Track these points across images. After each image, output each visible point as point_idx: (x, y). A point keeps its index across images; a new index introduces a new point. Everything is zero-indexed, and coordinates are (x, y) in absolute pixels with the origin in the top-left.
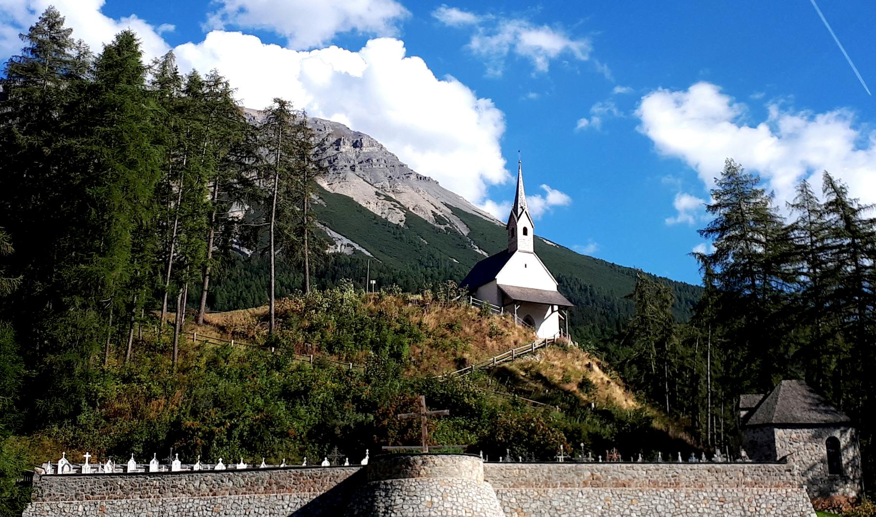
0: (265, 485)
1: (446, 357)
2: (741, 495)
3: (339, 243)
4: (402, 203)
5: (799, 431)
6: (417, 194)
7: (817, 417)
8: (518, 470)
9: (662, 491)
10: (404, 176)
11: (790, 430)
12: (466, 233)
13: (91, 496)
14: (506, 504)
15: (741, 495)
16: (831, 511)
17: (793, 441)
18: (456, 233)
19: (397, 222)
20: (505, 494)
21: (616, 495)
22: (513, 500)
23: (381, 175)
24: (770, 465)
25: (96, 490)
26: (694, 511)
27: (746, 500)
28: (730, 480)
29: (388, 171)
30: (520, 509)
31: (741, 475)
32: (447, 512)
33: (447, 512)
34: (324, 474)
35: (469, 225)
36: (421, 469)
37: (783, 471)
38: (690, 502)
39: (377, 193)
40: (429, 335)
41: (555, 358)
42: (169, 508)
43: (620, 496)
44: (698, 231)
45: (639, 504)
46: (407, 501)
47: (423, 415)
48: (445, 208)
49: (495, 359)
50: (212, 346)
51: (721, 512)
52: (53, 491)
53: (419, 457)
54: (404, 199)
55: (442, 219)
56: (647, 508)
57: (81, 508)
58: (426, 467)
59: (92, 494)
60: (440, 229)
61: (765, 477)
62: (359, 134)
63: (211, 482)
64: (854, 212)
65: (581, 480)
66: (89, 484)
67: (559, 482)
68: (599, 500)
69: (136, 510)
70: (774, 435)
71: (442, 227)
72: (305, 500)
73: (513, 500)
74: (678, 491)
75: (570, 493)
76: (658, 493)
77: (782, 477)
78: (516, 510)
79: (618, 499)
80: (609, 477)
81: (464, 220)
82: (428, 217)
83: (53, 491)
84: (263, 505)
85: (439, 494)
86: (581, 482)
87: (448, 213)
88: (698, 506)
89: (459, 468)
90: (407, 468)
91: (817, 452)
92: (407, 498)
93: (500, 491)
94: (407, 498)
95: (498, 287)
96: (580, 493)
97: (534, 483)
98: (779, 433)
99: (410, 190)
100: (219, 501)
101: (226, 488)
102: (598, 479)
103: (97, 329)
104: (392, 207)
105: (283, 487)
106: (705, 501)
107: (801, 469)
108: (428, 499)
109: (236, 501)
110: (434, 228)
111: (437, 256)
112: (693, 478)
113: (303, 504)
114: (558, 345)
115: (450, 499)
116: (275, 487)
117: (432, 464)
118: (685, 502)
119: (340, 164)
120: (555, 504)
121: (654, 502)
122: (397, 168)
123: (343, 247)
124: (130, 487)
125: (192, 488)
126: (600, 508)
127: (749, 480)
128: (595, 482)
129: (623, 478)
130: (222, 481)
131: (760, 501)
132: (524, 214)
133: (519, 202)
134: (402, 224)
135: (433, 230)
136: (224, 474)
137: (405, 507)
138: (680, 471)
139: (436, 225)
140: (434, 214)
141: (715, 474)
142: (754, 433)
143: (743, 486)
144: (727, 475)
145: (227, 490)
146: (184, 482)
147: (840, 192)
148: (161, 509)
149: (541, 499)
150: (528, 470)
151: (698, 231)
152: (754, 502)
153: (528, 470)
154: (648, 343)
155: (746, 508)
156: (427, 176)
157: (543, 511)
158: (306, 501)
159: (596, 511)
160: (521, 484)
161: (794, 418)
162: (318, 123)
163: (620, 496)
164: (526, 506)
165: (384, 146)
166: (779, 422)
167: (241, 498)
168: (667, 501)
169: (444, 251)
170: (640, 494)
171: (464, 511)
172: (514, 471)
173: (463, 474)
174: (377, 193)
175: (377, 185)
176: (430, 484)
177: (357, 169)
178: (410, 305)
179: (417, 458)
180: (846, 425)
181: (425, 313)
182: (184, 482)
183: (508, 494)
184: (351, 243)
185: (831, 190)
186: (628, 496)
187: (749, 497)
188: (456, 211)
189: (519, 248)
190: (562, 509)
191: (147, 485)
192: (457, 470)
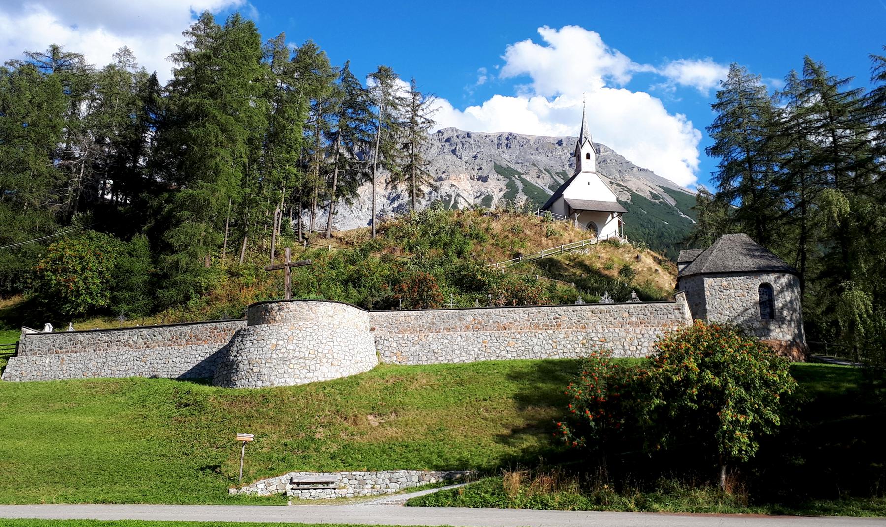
0: (186, 338)
1: (503, 253)
5: (729, 279)
7: (750, 263)
8: (403, 318)
9: (540, 332)
11: (721, 279)
12: (674, 204)
13: (59, 350)
14: (387, 349)
15: (623, 334)
17: (723, 289)
18: (666, 205)
19: (626, 200)
20: (387, 340)
21: (494, 338)
22: (394, 345)
23: (614, 170)
24: (657, 304)
25: (63, 346)
26: (571, 351)
28: (613, 321)
29: (618, 167)
30: (400, 353)
31: (626, 315)
34: (234, 327)
35: (677, 199)
36: (277, 315)
37: (672, 310)
38: (568, 342)
39: (611, 182)
40: (494, 236)
42: (109, 359)
43: (497, 338)
44: (706, 128)
45: (516, 346)
46: (255, 344)
47: (286, 265)
48: (659, 189)
49: (543, 254)
52: (33, 347)
53: (276, 304)
54: (630, 185)
56: (523, 349)
57: (48, 360)
58: (281, 313)
59: (61, 348)
61: (652, 316)
62: (597, 145)
63: (146, 336)
65: (463, 324)
66: (58, 340)
67: (442, 327)
68: (476, 342)
70: (703, 284)
71: (657, 201)
72: (214, 350)
73: (394, 345)
74: (557, 332)
75: (449, 337)
76: (537, 334)
77: (670, 316)
78: (396, 354)
79: (495, 341)
80: (491, 321)
81: (673, 195)
82: (648, 196)
83: (33, 347)
84: (180, 355)
85: (286, 337)
86: (463, 327)
87: (660, 191)
88: (576, 346)
89: (315, 314)
90: (265, 314)
91: (748, 298)
92: (256, 342)
93: (383, 337)
94: (256, 342)
95: (565, 202)
96: (459, 337)
97: (418, 329)
98: (708, 281)
99: (634, 178)
101: (157, 341)
102: (480, 323)
104: (621, 190)
105: (200, 339)
107: (731, 315)
108: (274, 342)
109: (160, 352)
110: (651, 202)
111: (653, 220)
112: (575, 319)
113: (211, 354)
114: (610, 242)
116: (194, 339)
117: (287, 310)
118: (563, 343)
121: (531, 343)
122: (624, 165)
124: (87, 342)
125: (132, 342)
126: (476, 350)
127: (634, 319)
128: (477, 326)
130: (154, 336)
131: (643, 340)
132: (587, 143)
133: (583, 133)
134: (629, 201)
136: (155, 329)
138: (563, 313)
139: (652, 200)
140: (651, 193)
141: (599, 315)
142: (686, 283)
143: (628, 326)
144: (611, 316)
145: (157, 343)
146: (126, 337)
148: (104, 360)
149: (421, 343)
150: (413, 317)
151: (706, 128)
152: (636, 341)
153: (413, 317)
154: (706, 242)
155: (627, 348)
157: (421, 355)
158: (215, 350)
159: (472, 353)
160: (406, 330)
161: (725, 267)
163: (497, 338)
164: (406, 349)
165: (615, 151)
166: (709, 271)
168: (545, 342)
169: (659, 217)
170: (518, 336)
171: (307, 353)
172: (400, 319)
173: (320, 319)
174: (611, 182)
175: (611, 177)
176: (280, 328)
179: (274, 305)
180: (782, 271)
182: (126, 337)
183: (390, 339)
186: (506, 338)
187: (630, 336)
188: (667, 190)
189: (583, 169)
190: (439, 352)
191: (99, 340)
192: (313, 315)
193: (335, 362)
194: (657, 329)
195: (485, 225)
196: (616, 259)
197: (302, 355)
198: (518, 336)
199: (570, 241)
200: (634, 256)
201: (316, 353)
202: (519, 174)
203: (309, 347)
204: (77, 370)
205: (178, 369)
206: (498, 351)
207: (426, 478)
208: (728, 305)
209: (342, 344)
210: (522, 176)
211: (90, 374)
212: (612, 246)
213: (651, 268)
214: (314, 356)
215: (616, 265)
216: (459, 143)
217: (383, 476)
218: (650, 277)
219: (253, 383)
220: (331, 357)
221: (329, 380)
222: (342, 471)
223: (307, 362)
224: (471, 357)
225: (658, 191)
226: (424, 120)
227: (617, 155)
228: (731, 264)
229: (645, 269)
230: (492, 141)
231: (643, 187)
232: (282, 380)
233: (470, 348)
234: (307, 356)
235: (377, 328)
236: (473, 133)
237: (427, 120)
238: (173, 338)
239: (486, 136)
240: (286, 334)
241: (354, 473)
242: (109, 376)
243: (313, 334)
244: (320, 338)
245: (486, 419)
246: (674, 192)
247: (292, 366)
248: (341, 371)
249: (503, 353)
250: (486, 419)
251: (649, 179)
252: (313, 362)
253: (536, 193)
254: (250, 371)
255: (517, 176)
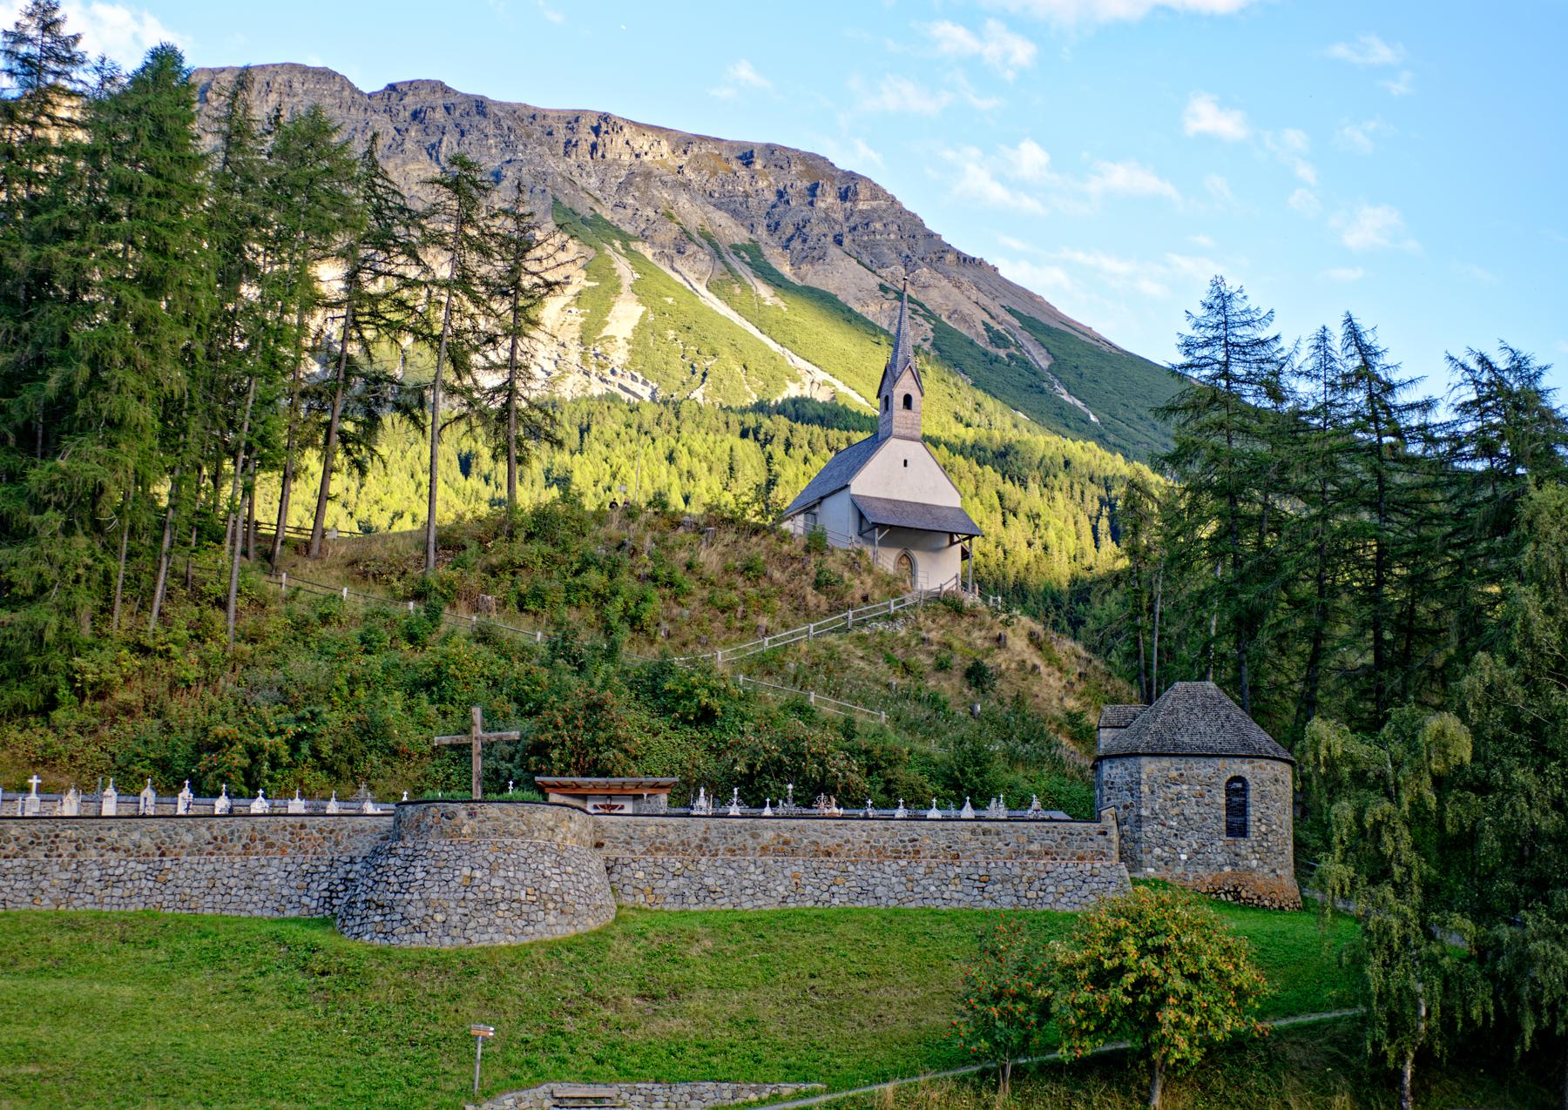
2: (1017, 871)
3: (807, 379)
4: (929, 307)
6: (957, 290)
10: (933, 256)
15: (1017, 871)
16: (1222, 896)
18: (1026, 364)
27: (1024, 880)
32: (494, 893)
33: (494, 893)
35: (1056, 352)
38: (930, 881)
41: (934, 626)
48: (1009, 318)
50: (310, 596)
51: (979, 898)
55: (1002, 338)
60: (997, 356)
62: (851, 176)
64: (1390, 388)
68: (781, 876)
69: (34, 875)
71: (1002, 353)
75: (735, 865)
79: (813, 875)
85: (486, 865)
99: (945, 282)
100: (168, 865)
103: (88, 568)
106: (957, 881)
108: (467, 871)
110: (985, 354)
112: (943, 843)
114: (945, 603)
115: (502, 873)
116: (259, 846)
119: (815, 232)
120: (709, 881)
123: (816, 385)
126: (781, 889)
127: (1035, 847)
129: (828, 842)
130: (176, 834)
135: (982, 358)
137: (428, 884)
139: (990, 349)
140: (988, 328)
141: (982, 838)
143: (1026, 857)
147: (1365, 351)
156: (978, 256)
159: (774, 894)
160: (658, 849)
161: (1176, 746)
162: (777, 153)
164: (661, 883)
167: (202, 861)
168: (894, 880)
170: (851, 868)
171: (523, 893)
173: (536, 834)
174: (882, 288)
177: (846, 241)
178: (681, 530)
181: (703, 546)
184: (831, 379)
185: (1353, 349)
187: (1029, 874)
188: (1030, 324)
192: (524, 828)
193: (567, 909)
194: (1070, 865)
195: (683, 555)
196: (956, 644)
197: (516, 896)
198: (851, 868)
199: (865, 599)
200: (991, 634)
201: (537, 893)
202: (626, 239)
203: (526, 882)
204: (16, 892)
205: (234, 899)
206: (817, 893)
207: (744, 1094)
208: (1176, 811)
209: (574, 878)
210: (633, 245)
211: (47, 901)
212: (949, 611)
213: (1024, 661)
214: (534, 898)
215: (957, 659)
216: (450, 126)
217: (680, 1090)
218: (1023, 684)
219: (435, 940)
220: (559, 899)
221: (559, 937)
222: (618, 1082)
223: (525, 908)
224: (772, 901)
225: (1007, 323)
226: (540, 282)
227: (902, 211)
228: (1186, 739)
229: (1013, 665)
230: (550, 134)
231: (967, 308)
232: (486, 937)
233: (771, 885)
234: (523, 896)
235: (607, 843)
236: (495, 103)
237: (545, 281)
238: (216, 838)
239: (534, 117)
240: (485, 859)
241: (638, 1085)
242: (89, 907)
243: (530, 861)
244: (541, 867)
245: (818, 1007)
246: (1048, 330)
247: (500, 913)
248: (575, 922)
249: (826, 896)
250: (818, 1007)
251: (985, 287)
252: (534, 908)
253: (670, 300)
254: (429, 920)
255: (617, 244)
